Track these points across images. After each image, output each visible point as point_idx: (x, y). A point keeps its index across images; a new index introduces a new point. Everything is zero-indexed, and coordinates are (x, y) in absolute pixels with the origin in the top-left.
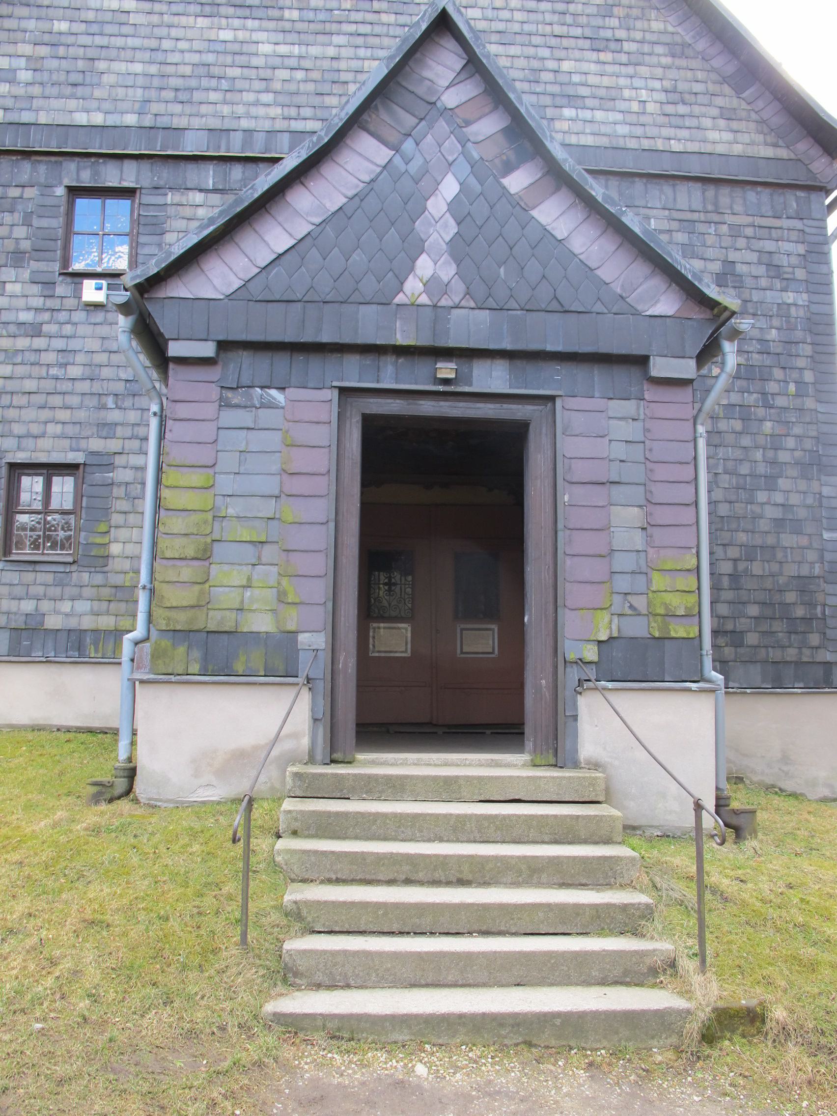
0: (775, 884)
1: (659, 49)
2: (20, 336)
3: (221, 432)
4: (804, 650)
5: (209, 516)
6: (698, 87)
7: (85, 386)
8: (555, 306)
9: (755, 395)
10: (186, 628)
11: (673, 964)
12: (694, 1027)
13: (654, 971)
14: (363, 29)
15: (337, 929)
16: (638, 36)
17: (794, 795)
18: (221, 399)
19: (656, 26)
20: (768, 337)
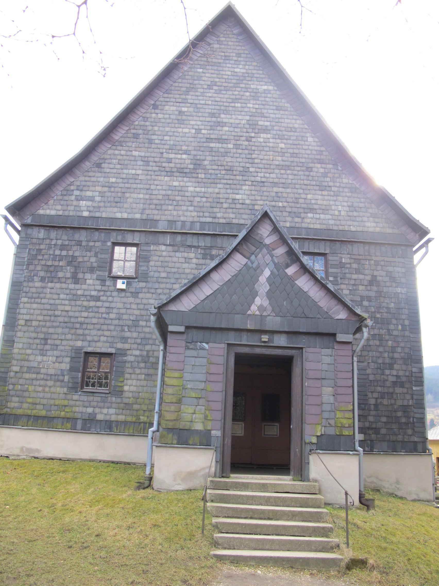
0: (377, 524)
1: (346, 190)
2: (91, 301)
3: (186, 358)
4: (405, 436)
5: (181, 388)
6: (362, 205)
7: (116, 322)
8: (303, 315)
9: (384, 330)
10: (172, 427)
11: (338, 546)
12: (343, 564)
13: (332, 548)
14: (229, 182)
15: (229, 532)
16: (338, 184)
17: (401, 498)
18: (186, 346)
19: (345, 181)
20: (390, 306)
